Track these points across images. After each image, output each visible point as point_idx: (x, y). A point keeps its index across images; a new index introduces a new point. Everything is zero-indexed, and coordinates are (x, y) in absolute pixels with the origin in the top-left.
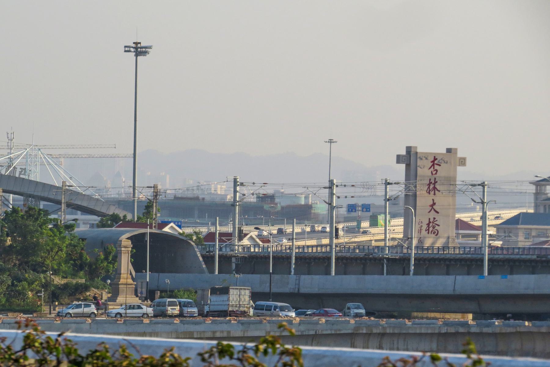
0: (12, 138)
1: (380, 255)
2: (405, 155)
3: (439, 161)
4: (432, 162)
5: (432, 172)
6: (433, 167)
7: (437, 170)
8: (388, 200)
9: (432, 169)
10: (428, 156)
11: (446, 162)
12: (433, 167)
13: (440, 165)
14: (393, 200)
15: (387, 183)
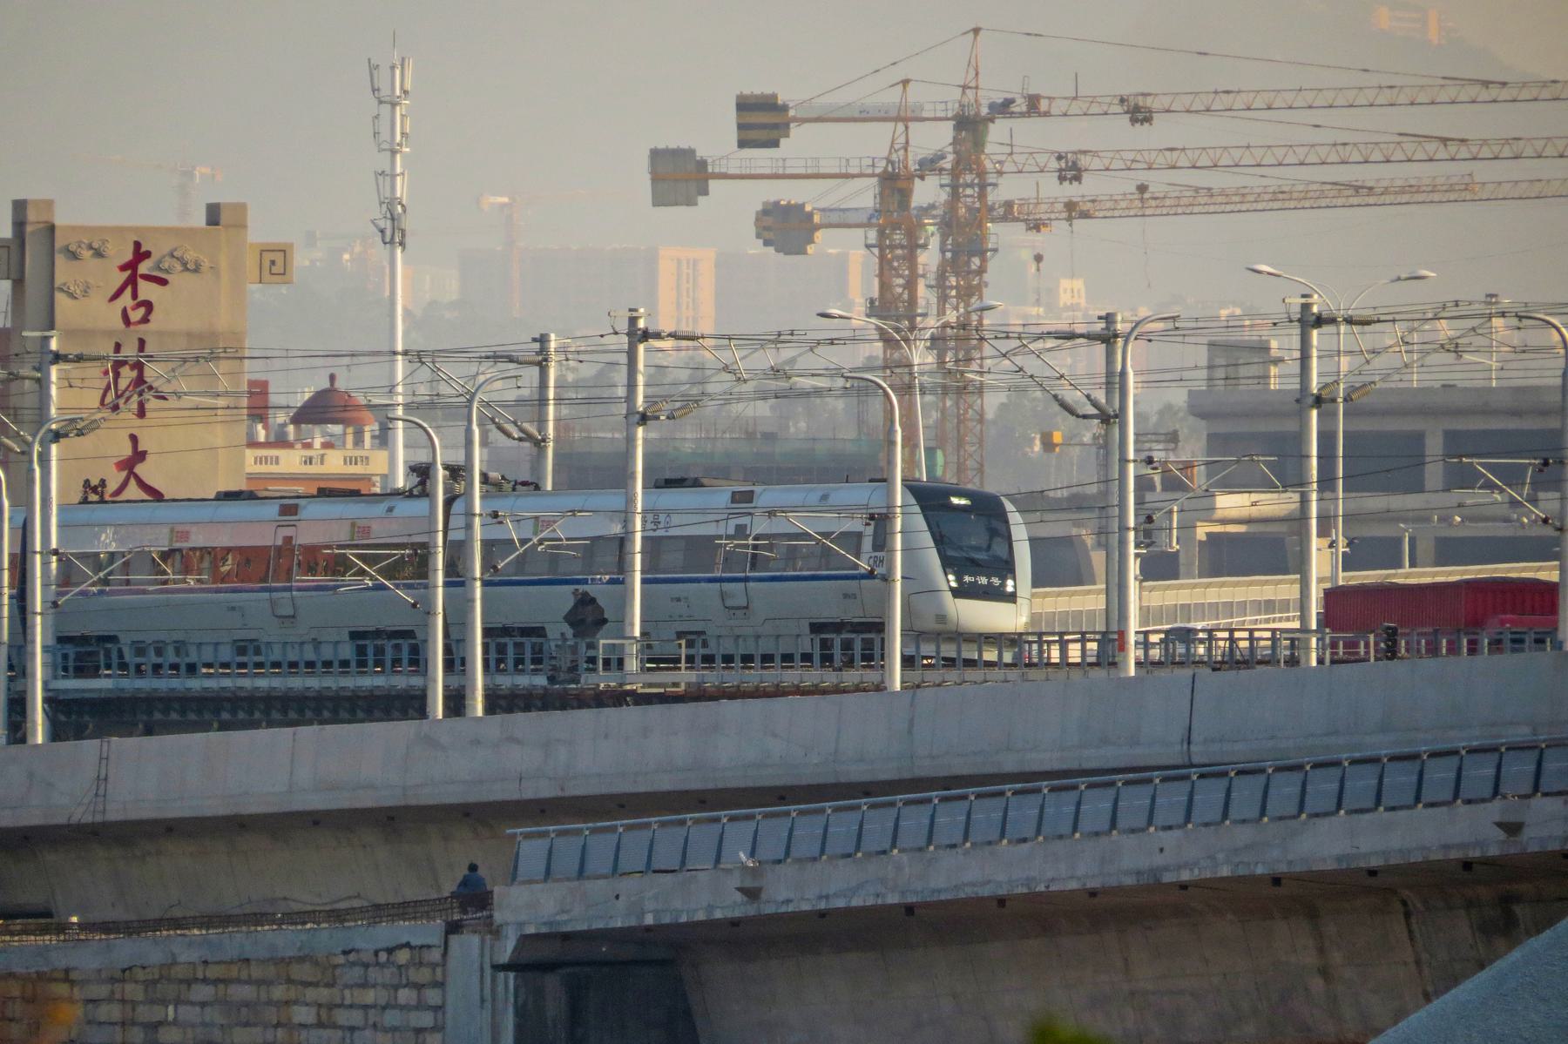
0: (398, 92)
1: (598, 685)
2: (8, 239)
3: (160, 261)
4: (123, 268)
5: (125, 314)
6: (128, 291)
7: (148, 306)
8: (644, 419)
9: (126, 299)
10: (104, 241)
11: (191, 266)
12: (128, 291)
13: (163, 282)
14: (662, 418)
15: (1311, 321)
